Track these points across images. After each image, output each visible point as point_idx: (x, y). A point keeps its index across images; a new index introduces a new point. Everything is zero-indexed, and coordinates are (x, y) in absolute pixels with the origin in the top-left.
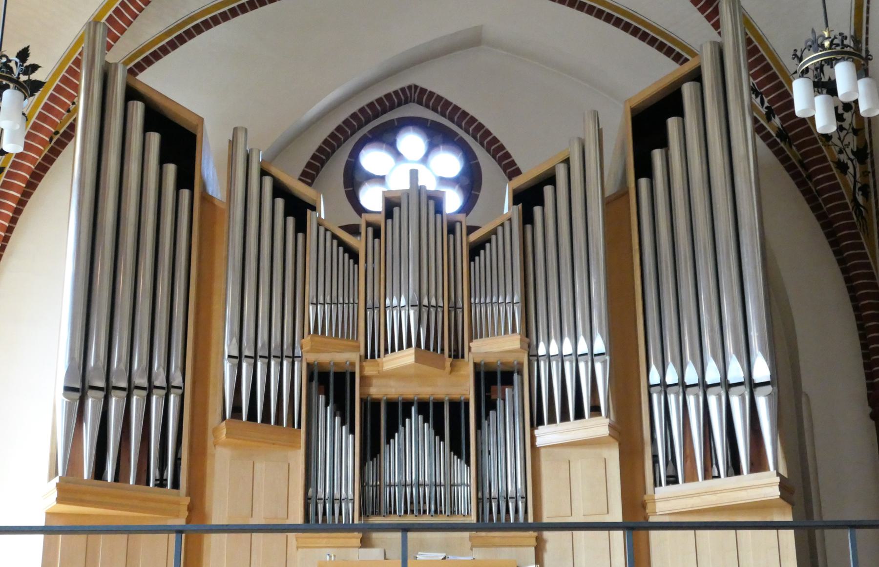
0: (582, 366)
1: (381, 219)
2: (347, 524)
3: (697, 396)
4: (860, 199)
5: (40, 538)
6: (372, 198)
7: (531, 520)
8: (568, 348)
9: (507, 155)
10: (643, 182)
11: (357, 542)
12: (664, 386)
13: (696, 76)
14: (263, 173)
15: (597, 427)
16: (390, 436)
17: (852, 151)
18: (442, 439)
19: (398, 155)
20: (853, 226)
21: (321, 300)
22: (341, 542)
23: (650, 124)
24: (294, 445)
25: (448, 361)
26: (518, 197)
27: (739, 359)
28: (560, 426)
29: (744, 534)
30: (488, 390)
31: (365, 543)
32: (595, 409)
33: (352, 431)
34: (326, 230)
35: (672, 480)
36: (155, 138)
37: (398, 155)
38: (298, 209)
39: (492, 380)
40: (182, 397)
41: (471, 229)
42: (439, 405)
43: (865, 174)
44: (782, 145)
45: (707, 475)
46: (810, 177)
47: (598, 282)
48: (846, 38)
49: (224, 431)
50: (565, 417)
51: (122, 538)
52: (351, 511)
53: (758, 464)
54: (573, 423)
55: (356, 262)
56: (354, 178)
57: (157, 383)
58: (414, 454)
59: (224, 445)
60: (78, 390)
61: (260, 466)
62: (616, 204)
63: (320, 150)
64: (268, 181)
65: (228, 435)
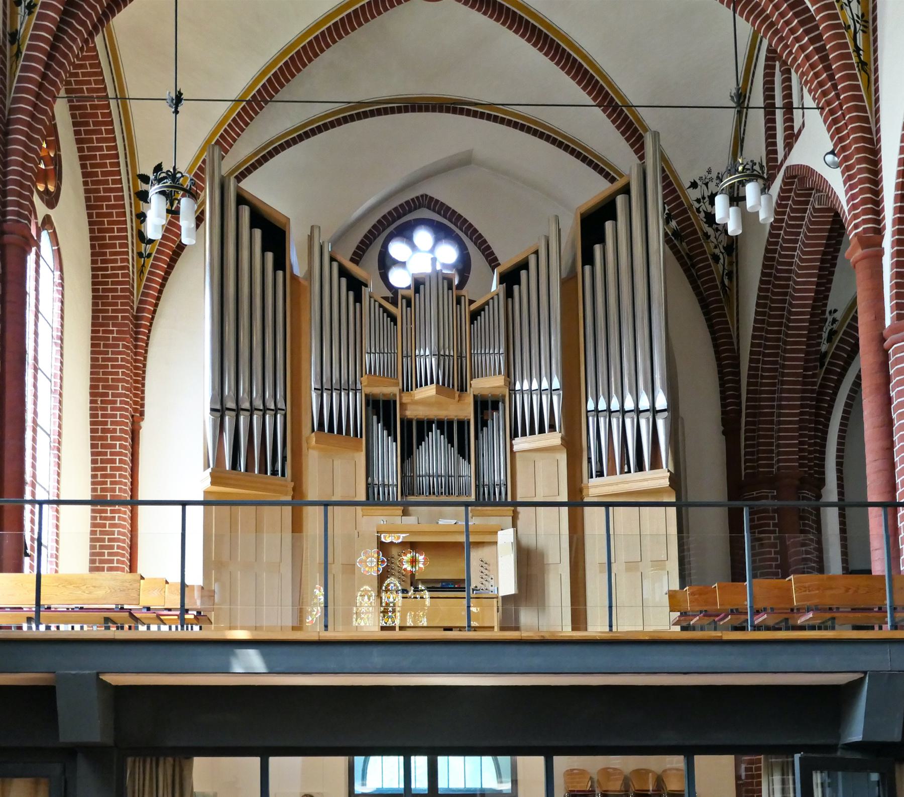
0: (544, 398)
1: (411, 293)
2: (393, 500)
3: (618, 419)
4: (726, 282)
5: (201, 508)
6: (400, 279)
7: (509, 499)
8: (535, 386)
9: (489, 247)
10: (587, 268)
11: (400, 512)
12: (597, 411)
13: (626, 190)
14: (332, 259)
15: (554, 439)
16: (419, 444)
17: (724, 248)
18: (452, 446)
19: (413, 247)
20: (720, 301)
21: (373, 351)
22: (386, 512)
23: (594, 223)
24: (358, 449)
25: (457, 393)
26: (503, 279)
27: (631, 393)
28: (529, 438)
29: (645, 510)
30: (482, 413)
31: (405, 513)
32: (552, 427)
33: (395, 440)
34: (375, 301)
35: (600, 474)
36: (258, 233)
37: (413, 247)
38: (356, 286)
39: (486, 406)
40: (285, 416)
41: (471, 302)
42: (450, 423)
43: (731, 263)
44: (676, 242)
45: (622, 472)
46: (693, 266)
47: (556, 340)
48: (755, 164)
49: (314, 439)
50: (532, 432)
51: (252, 509)
52: (395, 493)
53: (656, 464)
54: (537, 436)
55: (395, 324)
56: (385, 263)
57: (243, 407)
58: (433, 457)
59: (313, 448)
60: (219, 411)
61: (337, 463)
62: (569, 282)
63: (362, 242)
64: (335, 265)
65: (317, 442)
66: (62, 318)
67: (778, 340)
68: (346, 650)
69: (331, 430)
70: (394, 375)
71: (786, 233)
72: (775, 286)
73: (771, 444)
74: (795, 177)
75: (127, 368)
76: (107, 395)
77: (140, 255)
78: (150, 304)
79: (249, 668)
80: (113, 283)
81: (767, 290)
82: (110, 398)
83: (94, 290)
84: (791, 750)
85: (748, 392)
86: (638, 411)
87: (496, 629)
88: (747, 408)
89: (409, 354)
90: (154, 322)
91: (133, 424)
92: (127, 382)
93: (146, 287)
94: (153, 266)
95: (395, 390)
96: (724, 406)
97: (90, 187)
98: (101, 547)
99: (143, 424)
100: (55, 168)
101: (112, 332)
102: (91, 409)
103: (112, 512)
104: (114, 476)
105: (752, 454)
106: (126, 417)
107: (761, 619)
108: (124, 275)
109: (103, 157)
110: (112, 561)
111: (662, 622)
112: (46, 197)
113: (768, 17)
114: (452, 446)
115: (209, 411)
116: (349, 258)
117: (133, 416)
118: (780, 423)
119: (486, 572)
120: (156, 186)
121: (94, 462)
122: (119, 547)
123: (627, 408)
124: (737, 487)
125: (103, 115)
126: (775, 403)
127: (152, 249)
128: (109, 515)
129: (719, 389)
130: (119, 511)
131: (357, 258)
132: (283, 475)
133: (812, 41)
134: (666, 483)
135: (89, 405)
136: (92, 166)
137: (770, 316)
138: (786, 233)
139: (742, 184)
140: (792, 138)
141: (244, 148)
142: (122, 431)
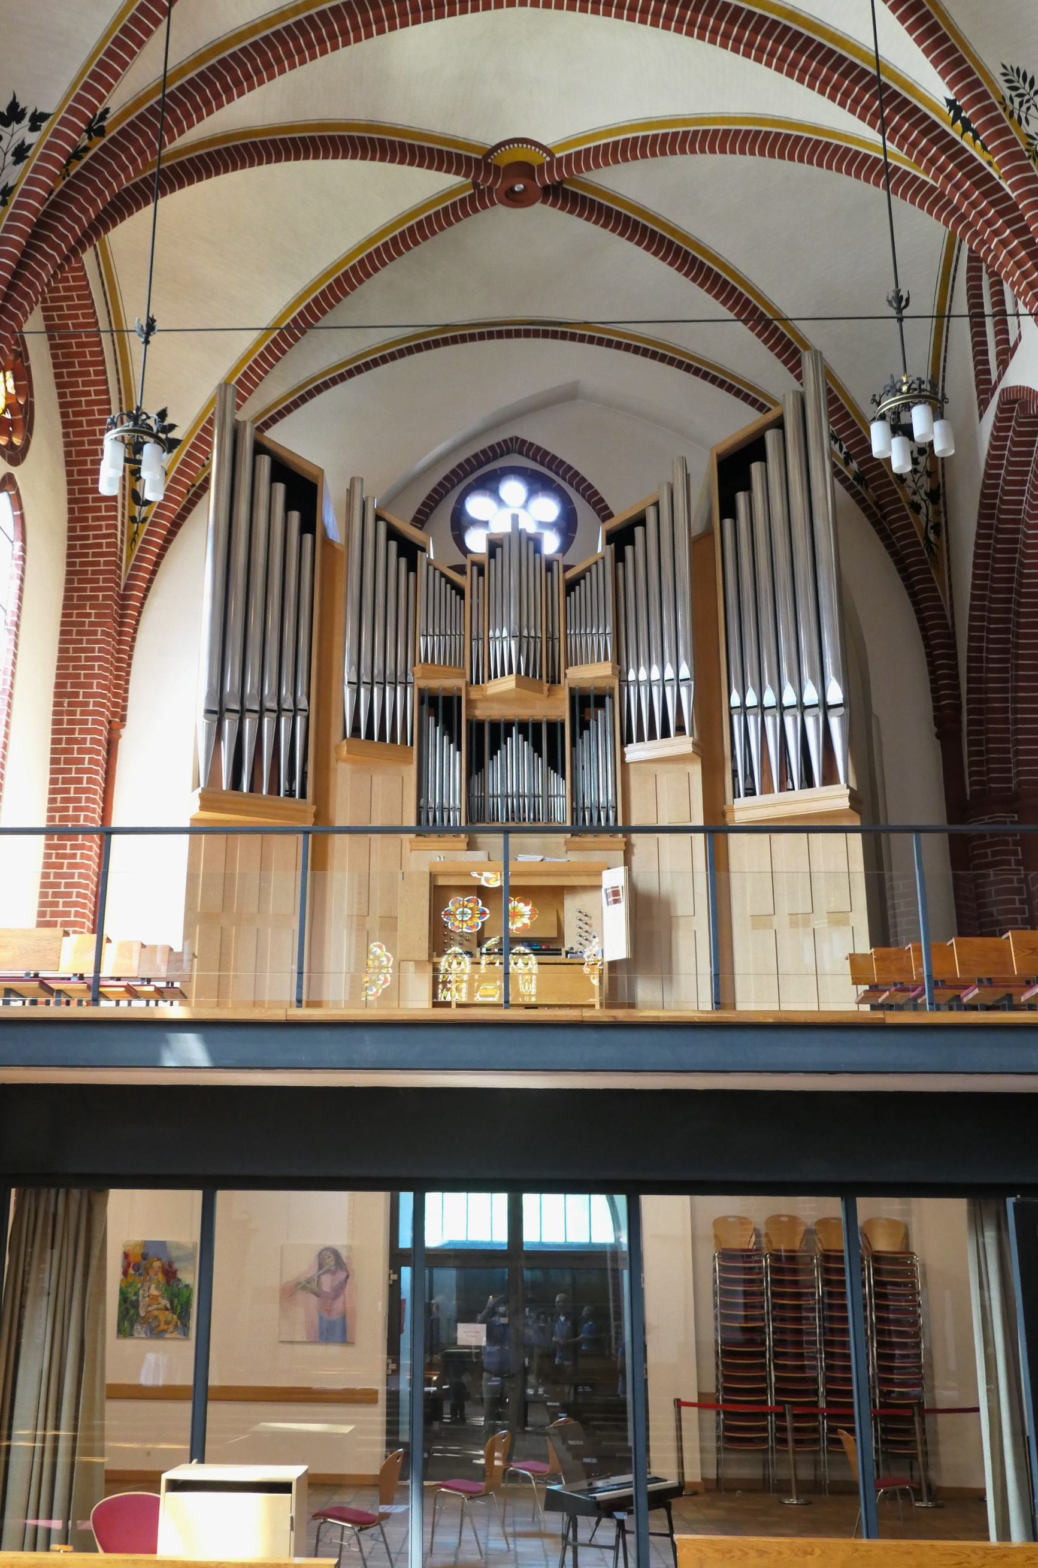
0: (668, 690)
4: (932, 537)
5: (186, 837)
6: (476, 542)
7: (620, 823)
10: (728, 522)
12: (744, 708)
13: (779, 424)
14: (378, 518)
15: (683, 745)
16: (493, 753)
17: (926, 493)
18: (540, 755)
19: (500, 502)
23: (735, 468)
25: (546, 686)
28: (647, 744)
30: (582, 712)
31: (471, 846)
32: (680, 729)
33: (459, 749)
34: (435, 569)
35: (750, 792)
36: (280, 488)
37: (500, 502)
39: (586, 703)
41: (567, 568)
42: (537, 725)
43: (937, 513)
44: (859, 487)
45: (782, 788)
46: (884, 517)
49: (345, 748)
50: (652, 736)
52: (459, 818)
53: (830, 778)
54: (659, 741)
55: (463, 598)
56: (460, 524)
58: (515, 770)
59: (345, 760)
60: (217, 712)
63: (429, 497)
66: (20, 599)
67: (1008, 611)
68: (325, 1034)
69: (370, 735)
70: (460, 664)
71: (1009, 473)
72: (998, 541)
73: (1007, 751)
74: (1015, 401)
75: (106, 661)
76: (76, 695)
77: (133, 519)
78: (142, 579)
79: (188, 1060)
80: (95, 555)
81: (987, 546)
82: (81, 699)
83: (69, 564)
84: (1010, 1189)
85: (969, 680)
86: (802, 707)
87: (598, 1007)
88: (969, 701)
89: (481, 636)
90: (147, 602)
91: (110, 731)
92: (105, 678)
93: (139, 559)
94: (148, 533)
95: (460, 683)
96: (936, 700)
97: (72, 438)
98: (55, 895)
99: (123, 732)
100: (25, 418)
101: (89, 615)
102: (55, 713)
103: (73, 847)
104: (79, 800)
105: (979, 763)
106: (101, 723)
107: (971, 996)
108: (108, 545)
109: (89, 403)
110: (68, 914)
111: (843, 999)
112: (8, 452)
113: (956, 209)
114: (540, 755)
115: (202, 712)
116: (411, 517)
117: (110, 722)
118: (1016, 721)
119: (587, 928)
120: (114, 431)
121: (53, 781)
122: (79, 895)
123: (807, 701)
124: (959, 805)
125: (92, 354)
126: (1009, 695)
127: (149, 512)
128: (68, 851)
129: (928, 678)
130: (82, 847)
131: (420, 520)
132: (303, 795)
133: (1016, 234)
134: (845, 803)
135: (52, 709)
136: (76, 414)
137: (994, 580)
138: (1009, 473)
139: (908, 407)
140: (1006, 353)
141: (274, 388)
142: (93, 741)
